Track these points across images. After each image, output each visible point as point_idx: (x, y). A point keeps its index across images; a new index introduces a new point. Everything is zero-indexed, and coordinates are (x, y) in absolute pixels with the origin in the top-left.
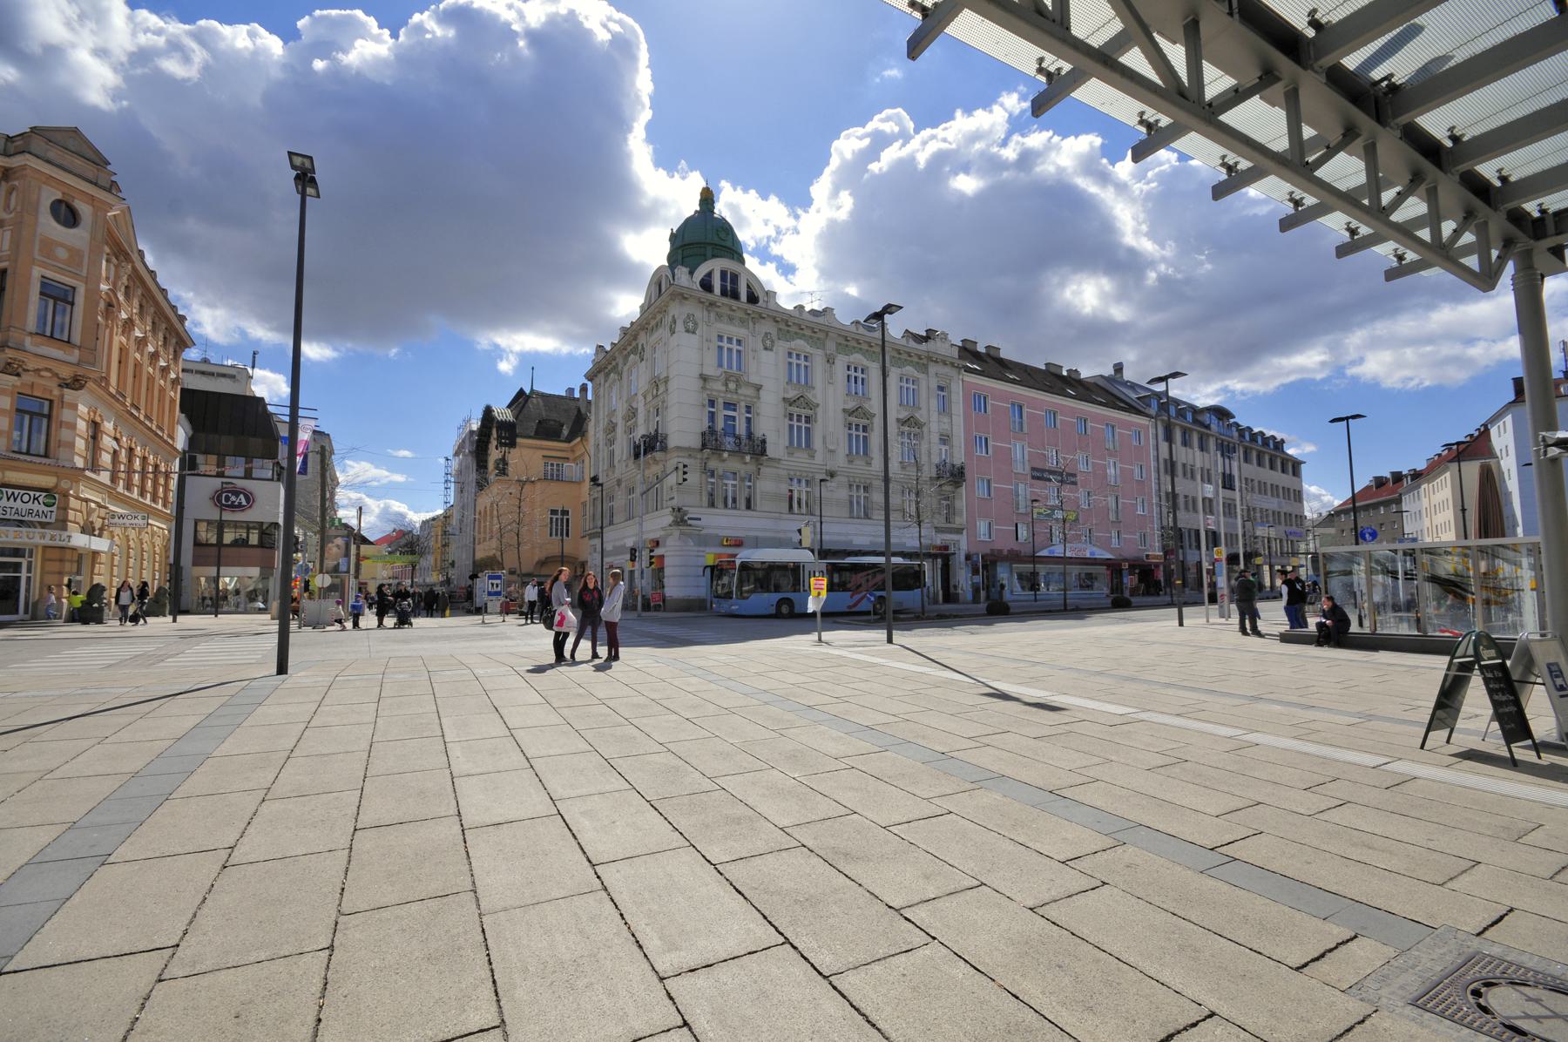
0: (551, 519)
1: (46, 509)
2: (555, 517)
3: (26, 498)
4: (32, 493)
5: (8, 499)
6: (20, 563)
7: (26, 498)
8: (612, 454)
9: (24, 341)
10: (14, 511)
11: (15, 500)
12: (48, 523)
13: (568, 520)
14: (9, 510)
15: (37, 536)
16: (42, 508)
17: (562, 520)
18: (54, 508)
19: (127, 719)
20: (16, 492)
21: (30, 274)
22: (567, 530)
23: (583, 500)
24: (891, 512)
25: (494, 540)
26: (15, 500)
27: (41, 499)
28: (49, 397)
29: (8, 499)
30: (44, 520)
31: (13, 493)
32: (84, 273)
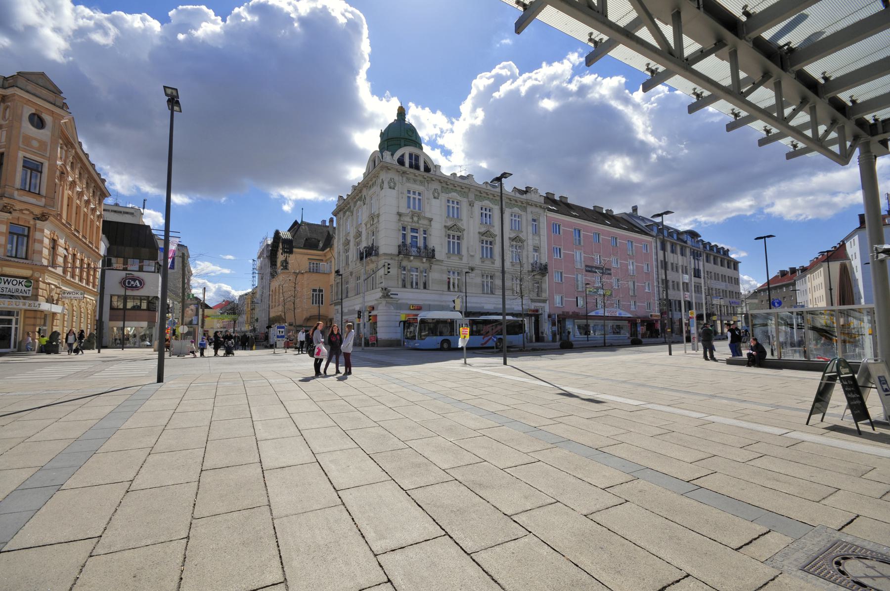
0: (313, 294)
1: (26, 289)
2: (315, 293)
3: (15, 282)
4: (18, 280)
5: (5, 283)
6: (12, 320)
7: (15, 282)
8: (347, 257)
9: (13, 193)
10: (8, 290)
11: (9, 284)
12: (27, 297)
13: (322, 295)
14: (5, 289)
15: (21, 304)
16: (24, 288)
17: (319, 295)
18: (31, 288)
19: (72, 408)
20: (9, 279)
21: (17, 156)
22: (322, 301)
23: (331, 284)
24: (506, 291)
25: (281, 306)
26: (9, 284)
27: (23, 283)
28: (28, 225)
29: (5, 283)
30: (25, 295)
31: (7, 280)
32: (48, 155)
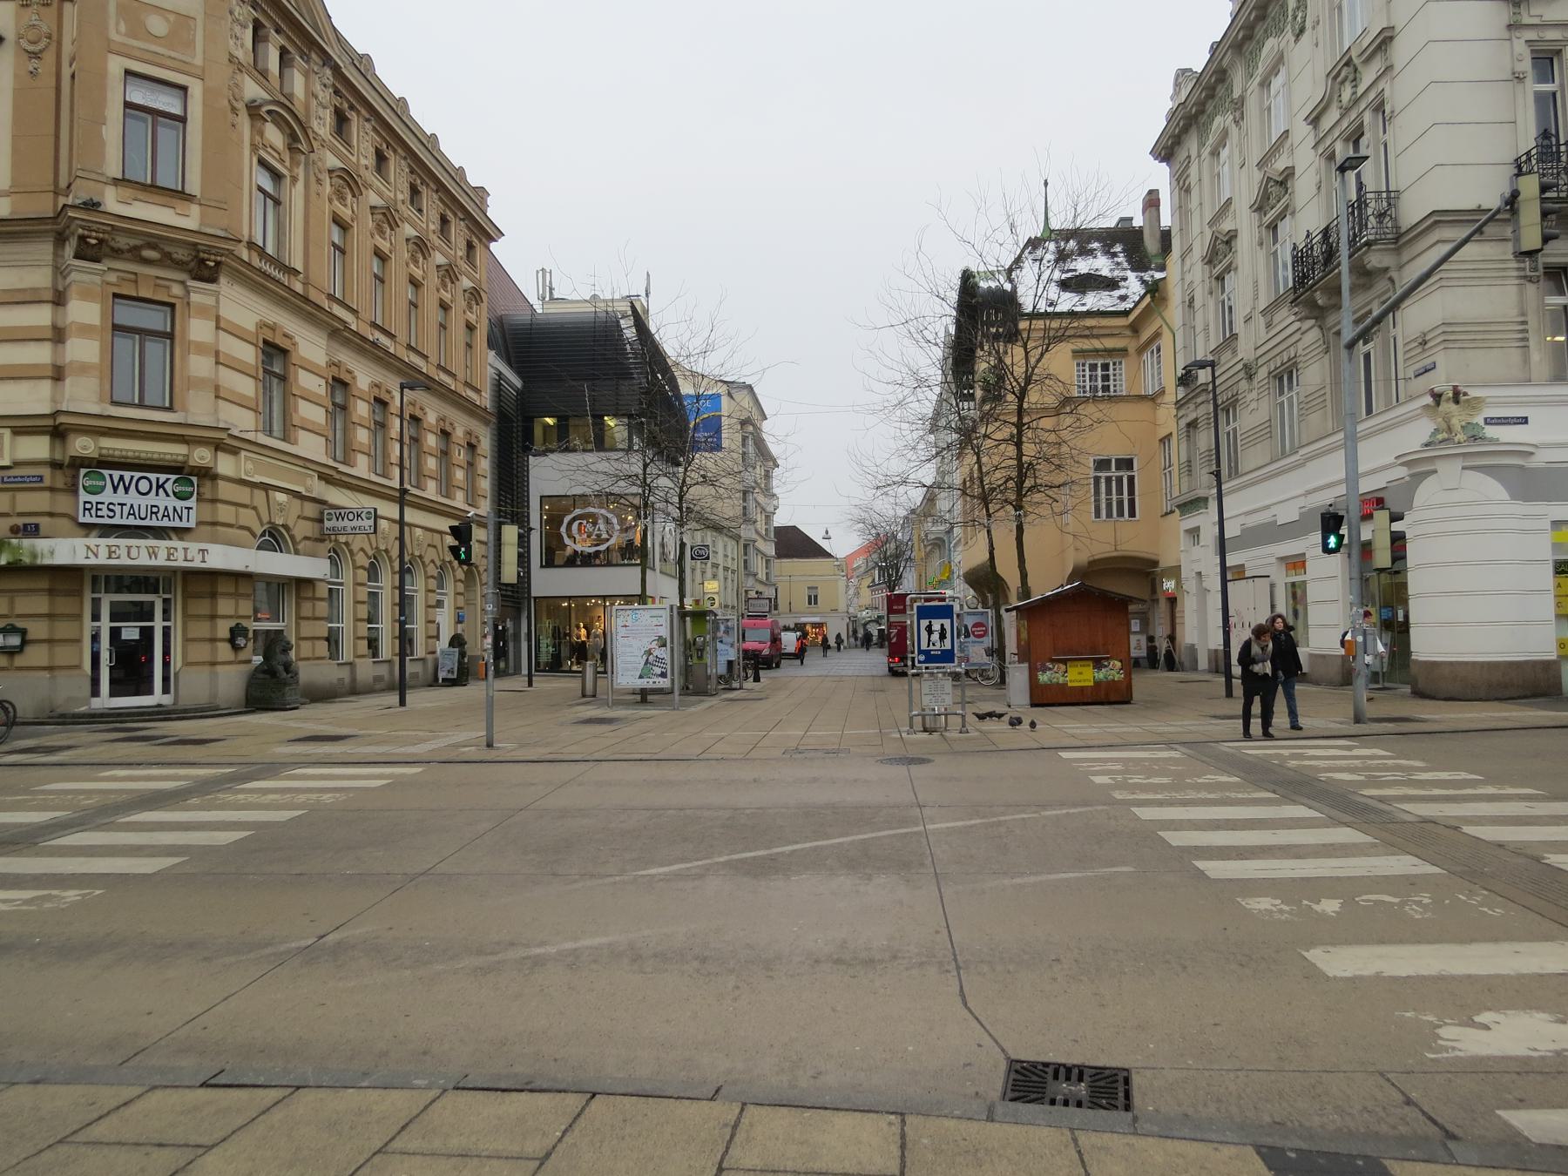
0: (1097, 480)
1: (179, 504)
2: (1103, 475)
3: (144, 486)
4: (152, 476)
5: (115, 489)
6: (152, 604)
7: (144, 486)
8: (1227, 310)
9: (102, 194)
10: (126, 509)
11: (127, 490)
12: (188, 530)
13: (1131, 480)
14: (117, 509)
15: (144, 552)
16: (172, 502)
17: (1119, 480)
18: (192, 502)
19: (513, 753)
20: (127, 475)
21: (105, 69)
22: (1097, 492)
23: (1162, 433)
24: (11, 493)
25: (957, 561)
26: (127, 490)
27: (168, 486)
28: (166, 299)
29: (115, 489)
30: (177, 523)
31: (122, 478)
32: (198, 61)
